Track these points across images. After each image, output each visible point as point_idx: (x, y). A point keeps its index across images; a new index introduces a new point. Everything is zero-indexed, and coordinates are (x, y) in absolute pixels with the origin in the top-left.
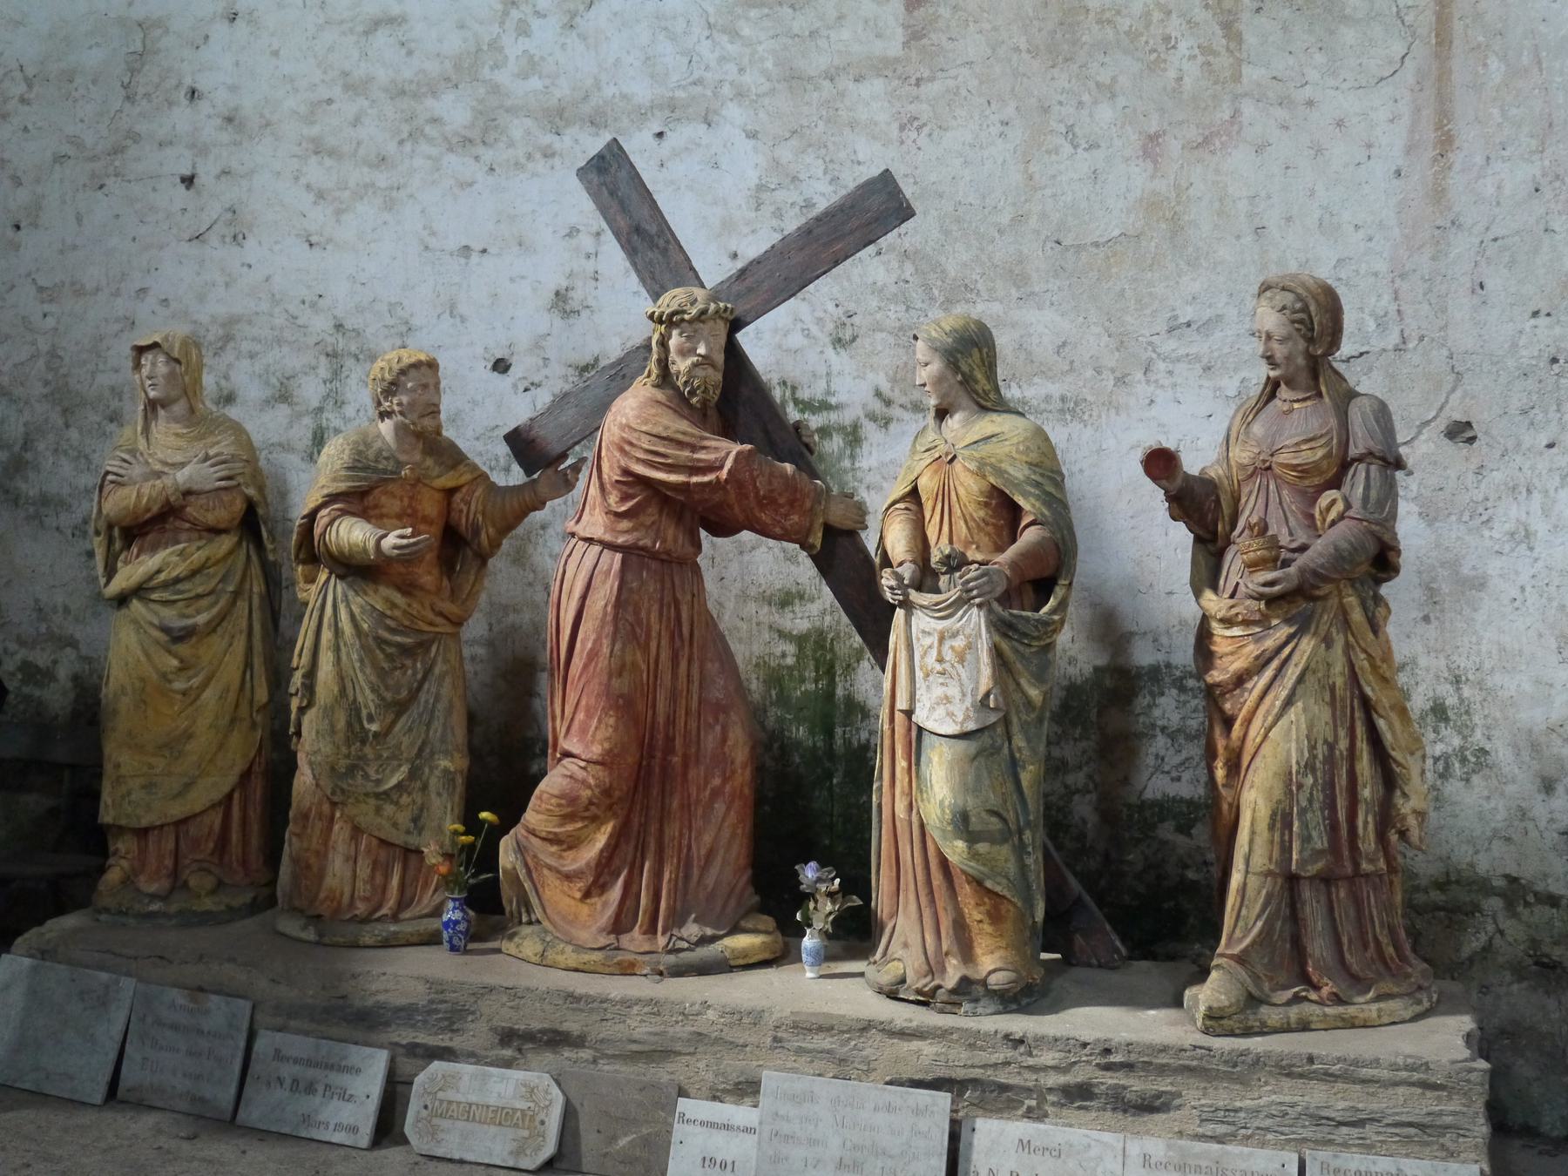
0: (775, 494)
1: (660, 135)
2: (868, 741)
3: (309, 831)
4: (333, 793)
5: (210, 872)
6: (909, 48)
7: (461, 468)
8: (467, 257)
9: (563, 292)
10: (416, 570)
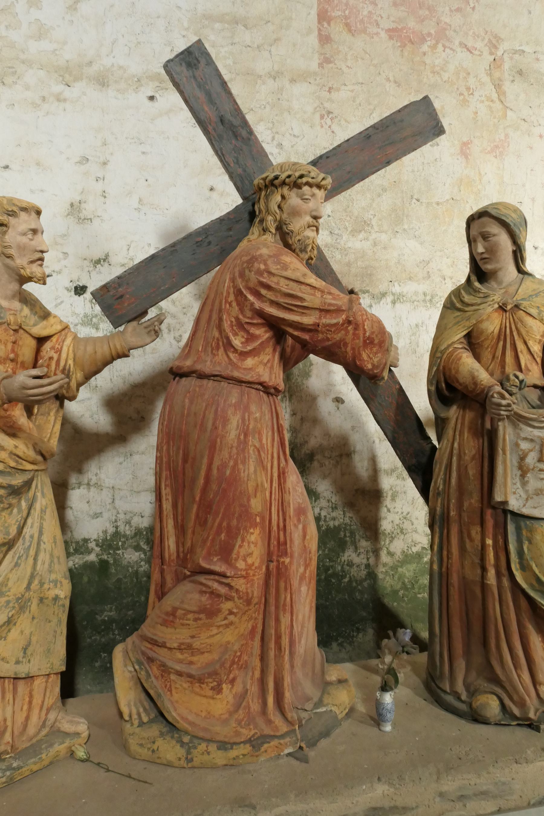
0: (374, 336)
1: (152, 98)
2: (320, 514)
6: (323, 67)
7: (51, 320)
9: (76, 204)
10: (13, 413)
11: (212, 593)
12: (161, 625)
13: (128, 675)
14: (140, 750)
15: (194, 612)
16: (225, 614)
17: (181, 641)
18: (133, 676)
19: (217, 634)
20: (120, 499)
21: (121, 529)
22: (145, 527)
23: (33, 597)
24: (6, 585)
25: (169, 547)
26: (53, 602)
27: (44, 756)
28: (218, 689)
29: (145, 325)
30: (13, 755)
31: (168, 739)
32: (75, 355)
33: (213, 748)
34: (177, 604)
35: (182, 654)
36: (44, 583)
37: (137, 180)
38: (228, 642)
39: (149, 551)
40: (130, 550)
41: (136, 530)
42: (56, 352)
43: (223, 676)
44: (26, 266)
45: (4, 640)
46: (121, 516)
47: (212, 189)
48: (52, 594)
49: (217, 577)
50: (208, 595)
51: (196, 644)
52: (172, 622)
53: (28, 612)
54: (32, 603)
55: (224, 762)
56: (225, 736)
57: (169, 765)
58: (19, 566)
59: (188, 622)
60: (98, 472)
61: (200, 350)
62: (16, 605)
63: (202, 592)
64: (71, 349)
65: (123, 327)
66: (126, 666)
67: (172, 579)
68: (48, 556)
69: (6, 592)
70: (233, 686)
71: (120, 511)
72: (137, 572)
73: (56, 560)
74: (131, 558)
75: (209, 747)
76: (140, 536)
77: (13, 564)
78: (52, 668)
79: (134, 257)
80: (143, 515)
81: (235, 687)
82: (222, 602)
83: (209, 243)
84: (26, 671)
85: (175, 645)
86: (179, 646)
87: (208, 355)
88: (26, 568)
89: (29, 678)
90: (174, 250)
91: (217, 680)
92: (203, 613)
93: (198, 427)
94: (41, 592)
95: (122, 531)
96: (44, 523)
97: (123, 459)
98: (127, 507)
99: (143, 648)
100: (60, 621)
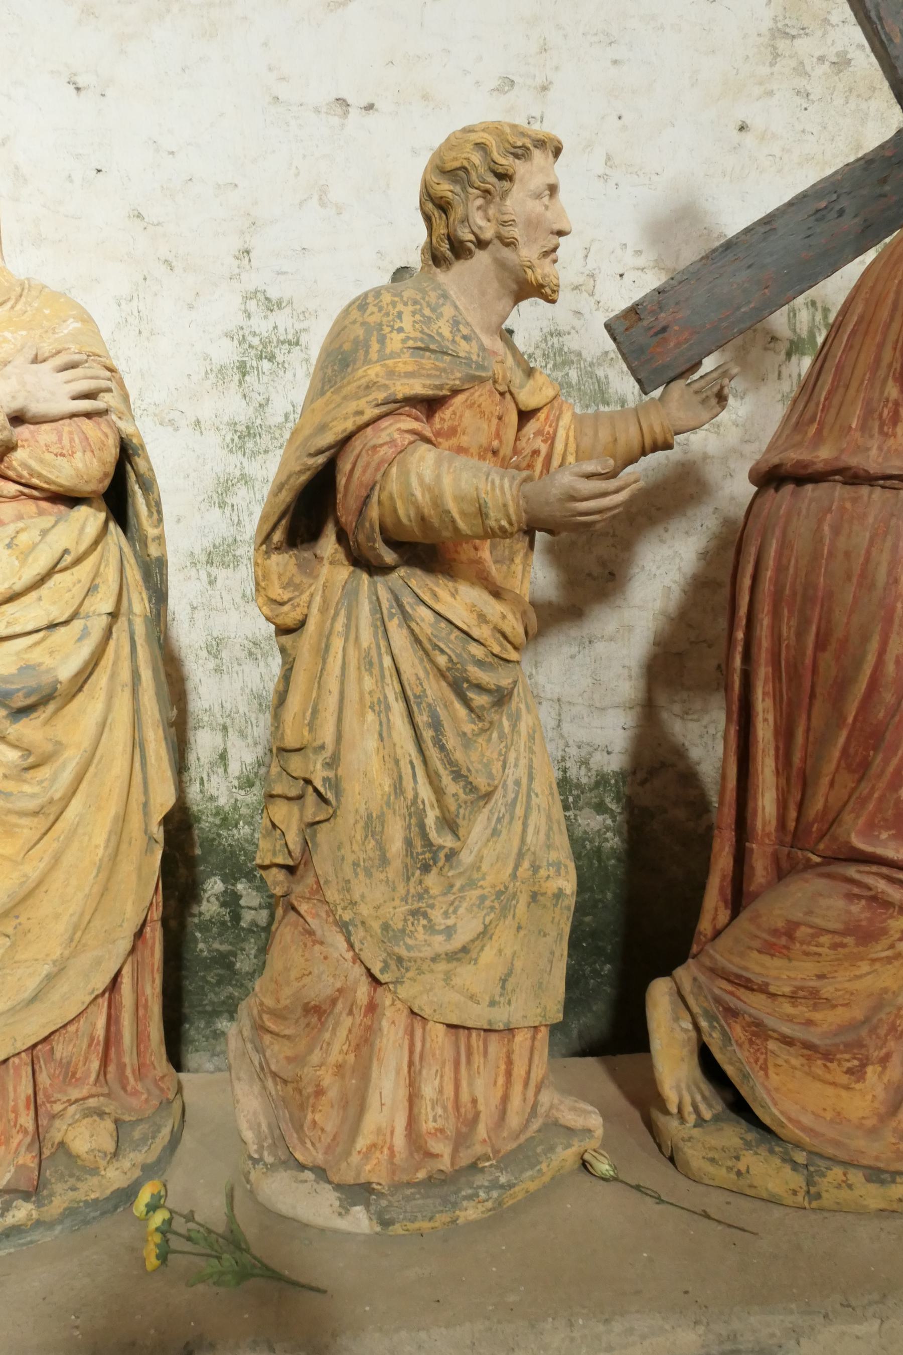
3: (327, 1036)
4: (385, 968)
5: (101, 1114)
8: (346, 113)
11: (874, 898)
12: (760, 952)
13: (680, 1036)
14: (711, 1169)
15: (834, 932)
16: (892, 939)
17: (798, 983)
18: (689, 1039)
19: (869, 973)
20: (571, 721)
21: (573, 773)
22: (613, 772)
23: (521, 892)
24: (479, 869)
25: (764, 808)
26: (554, 902)
27: (544, 1166)
28: (858, 1073)
29: (696, 386)
30: (494, 1162)
31: (763, 1154)
32: (577, 446)
33: (857, 1177)
34: (798, 916)
35: (794, 1005)
36: (539, 867)
37: (603, 118)
38: (885, 990)
39: (620, 813)
40: (587, 811)
41: (597, 775)
42: (544, 441)
43: (871, 1050)
44: (536, 262)
45: (475, 964)
46: (573, 751)
47: (742, 129)
48: (553, 886)
49: (885, 870)
50: (863, 902)
51: (827, 990)
52: (785, 947)
53: (510, 917)
54: (517, 902)
55: (882, 1206)
56: (877, 1158)
57: (773, 1201)
58: (499, 836)
59: (819, 950)
60: (534, 672)
61: (854, 426)
62: (496, 905)
63: (851, 897)
64: (572, 434)
65: (661, 389)
66: (676, 1019)
67: (766, 868)
68: (543, 820)
69: (479, 881)
70: (884, 1068)
71: (571, 742)
72: (599, 848)
73: (555, 827)
74: (588, 825)
75: (850, 1176)
76: (605, 787)
77: (489, 831)
78: (544, 1016)
79: (597, 271)
80: (610, 750)
81: (888, 1072)
82: (891, 917)
83: (841, 212)
84: (505, 1018)
85: (787, 990)
86: (794, 992)
87: (872, 436)
88: (510, 841)
89: (510, 1031)
90: (771, 230)
91: (860, 1056)
92: (849, 935)
93: (855, 580)
94: (534, 883)
95: (573, 777)
96: (535, 760)
97: (577, 649)
98: (581, 735)
99: (717, 992)
100: (560, 935)
